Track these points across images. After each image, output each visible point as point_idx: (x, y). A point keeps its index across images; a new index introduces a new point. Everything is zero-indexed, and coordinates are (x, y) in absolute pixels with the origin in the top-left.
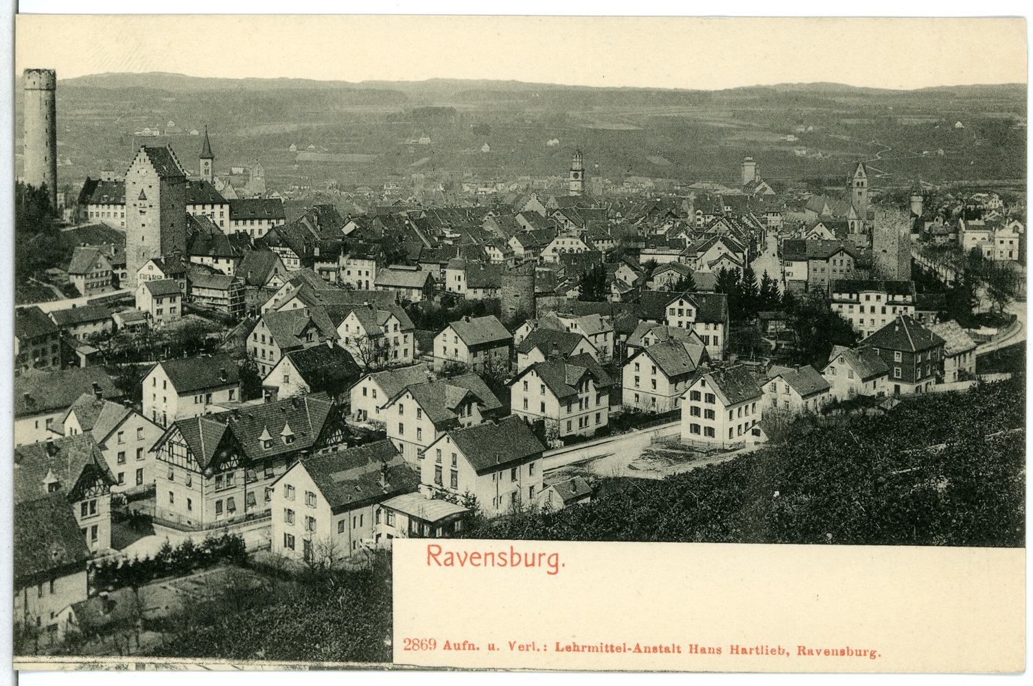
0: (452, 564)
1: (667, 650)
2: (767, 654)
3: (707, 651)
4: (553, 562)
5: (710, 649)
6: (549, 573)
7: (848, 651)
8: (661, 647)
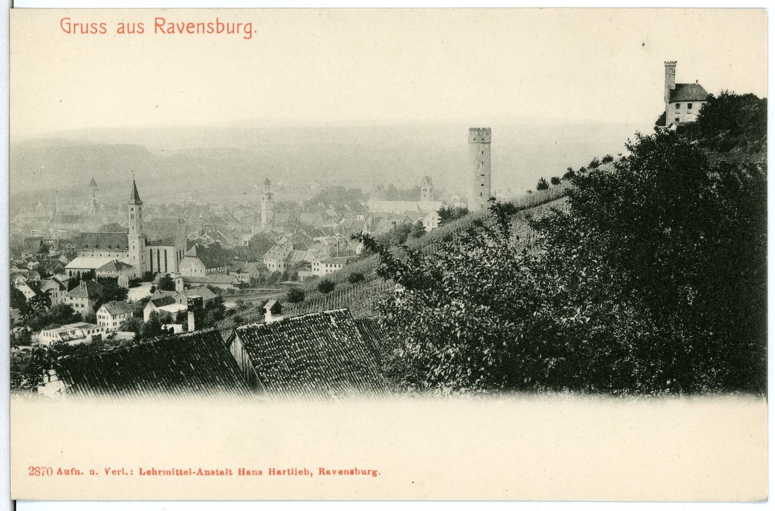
0: (173, 32)
1: (222, 473)
2: (296, 474)
3: (252, 473)
4: (248, 29)
5: (253, 471)
6: (245, 38)
7: (356, 471)
8: (217, 471)
